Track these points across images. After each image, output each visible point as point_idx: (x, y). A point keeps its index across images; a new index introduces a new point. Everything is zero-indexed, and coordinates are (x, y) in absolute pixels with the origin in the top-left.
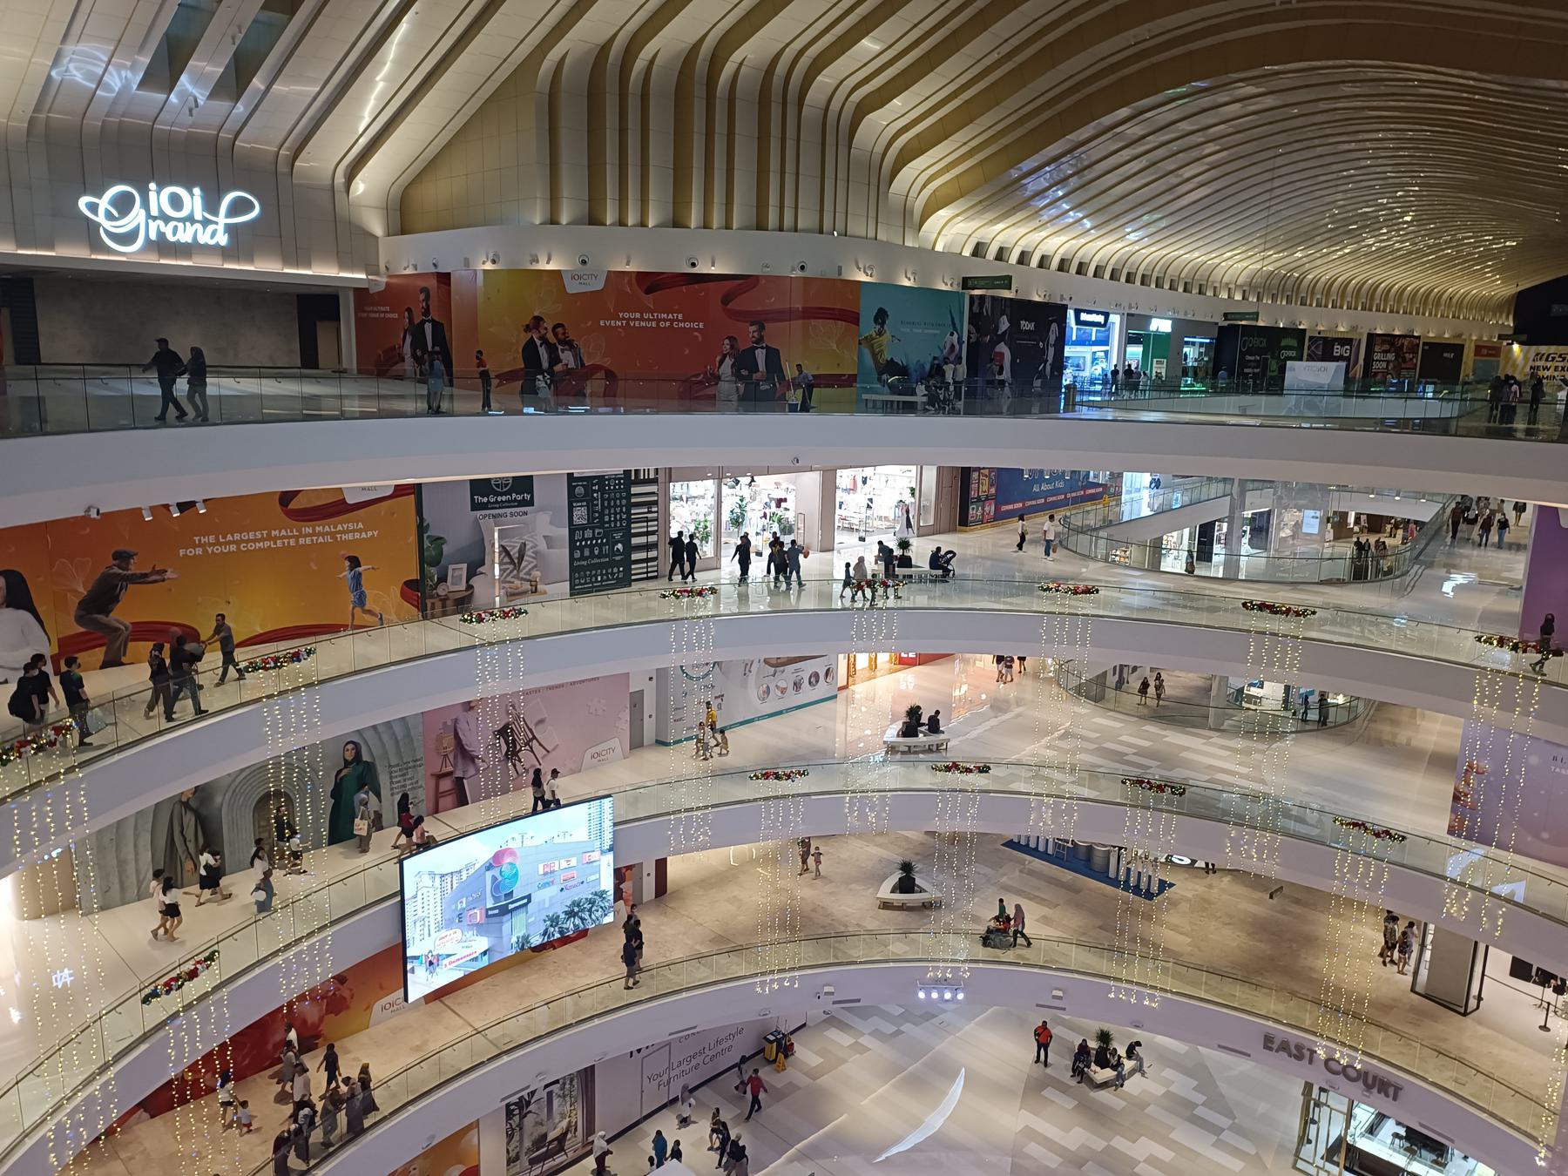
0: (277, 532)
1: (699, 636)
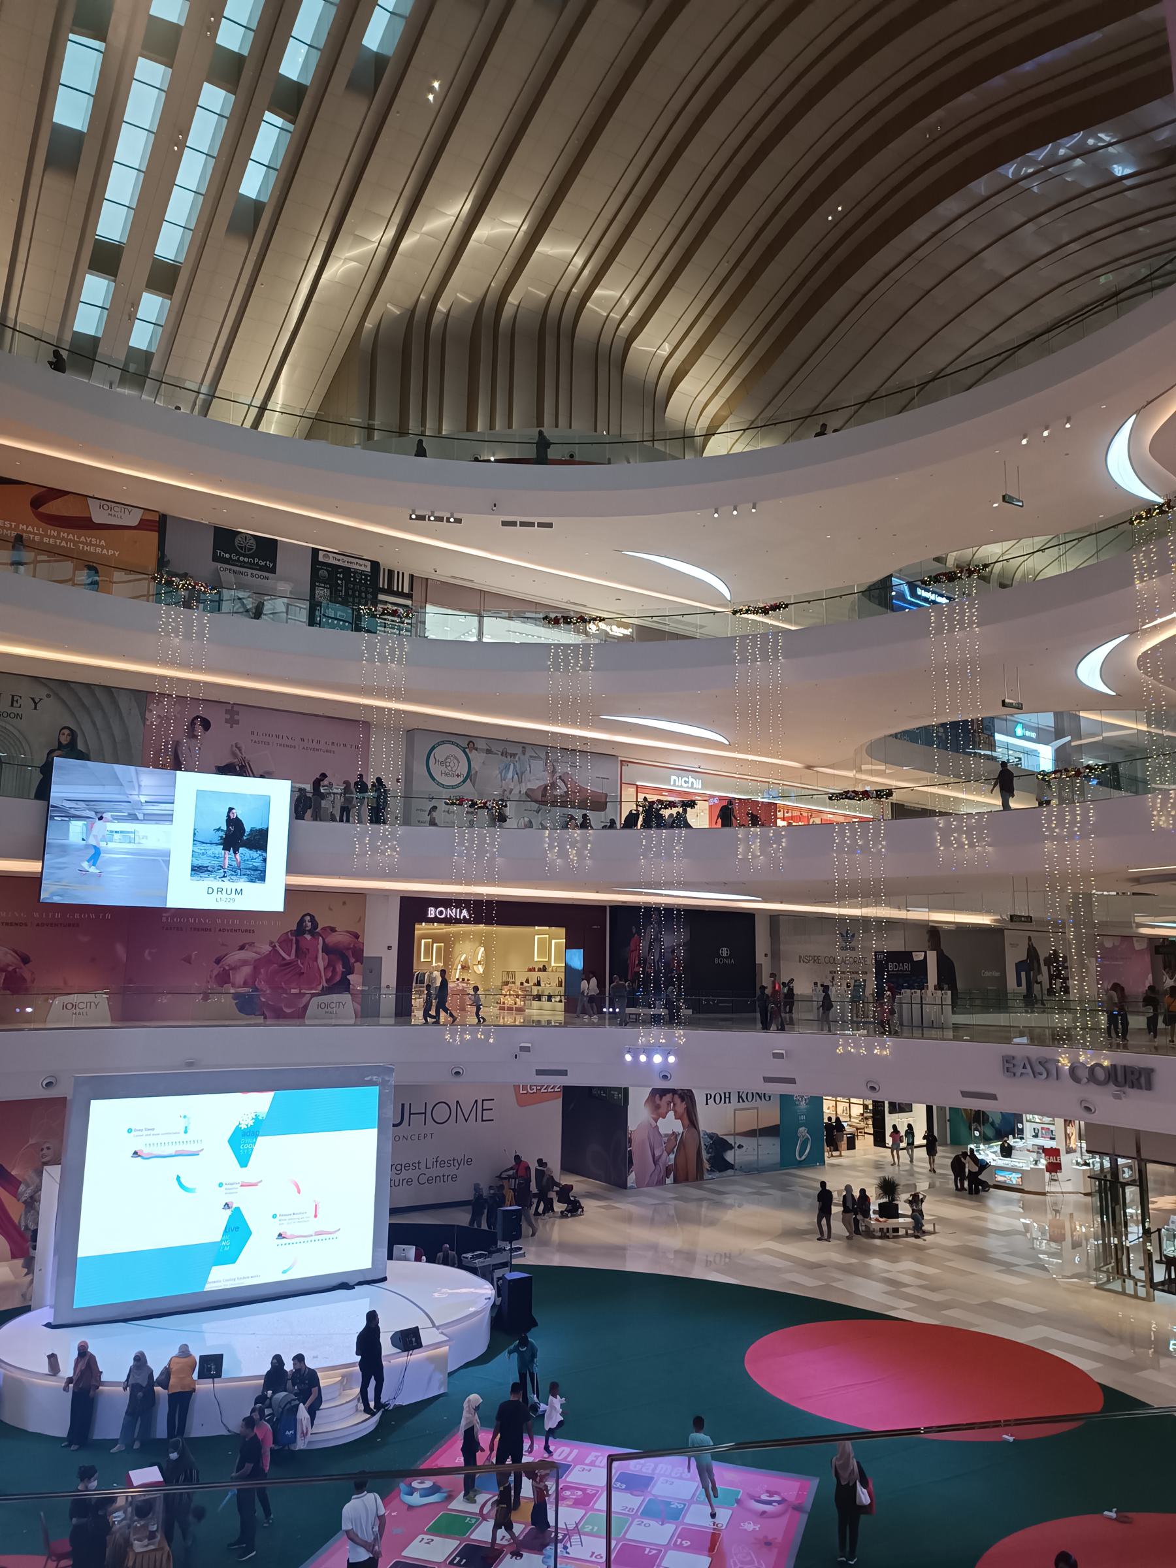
0: (25, 527)
1: (392, 650)
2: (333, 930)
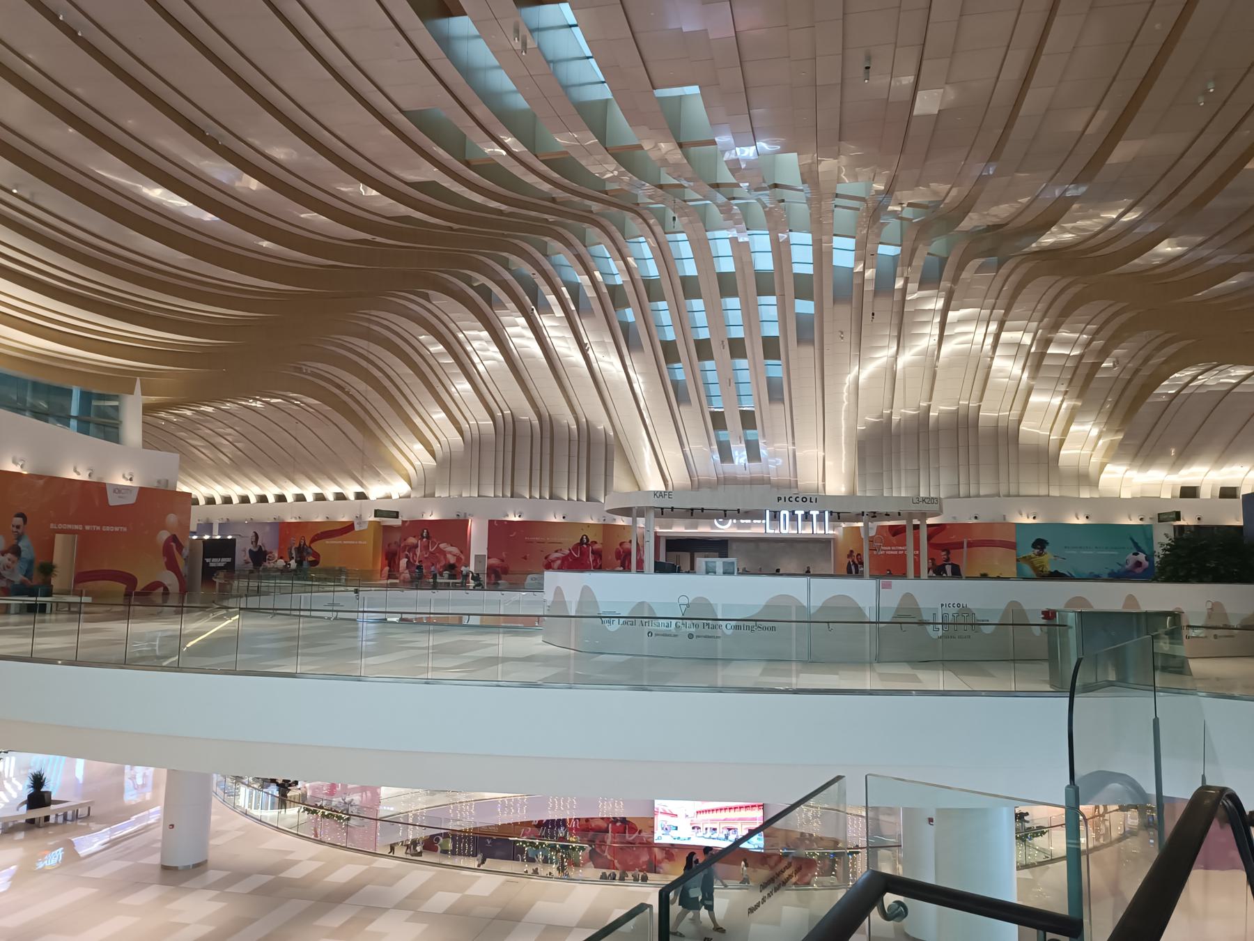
2: (596, 543)
